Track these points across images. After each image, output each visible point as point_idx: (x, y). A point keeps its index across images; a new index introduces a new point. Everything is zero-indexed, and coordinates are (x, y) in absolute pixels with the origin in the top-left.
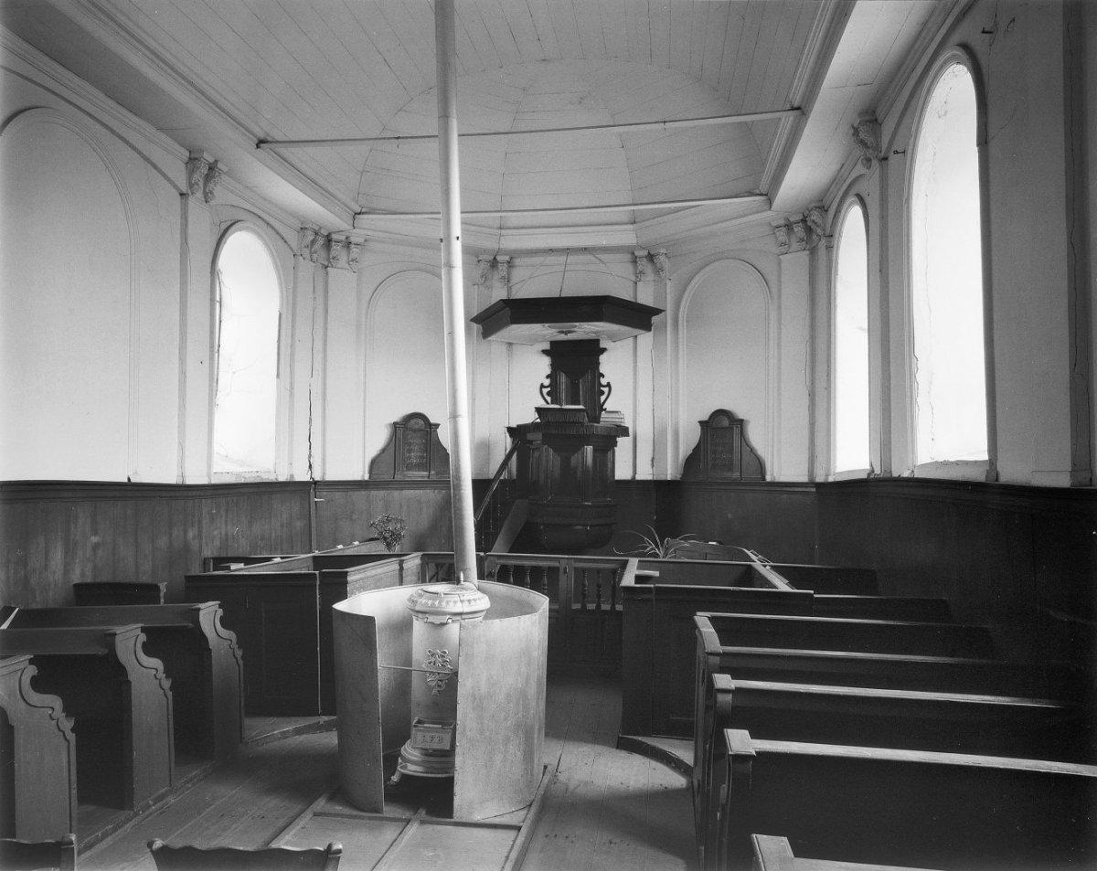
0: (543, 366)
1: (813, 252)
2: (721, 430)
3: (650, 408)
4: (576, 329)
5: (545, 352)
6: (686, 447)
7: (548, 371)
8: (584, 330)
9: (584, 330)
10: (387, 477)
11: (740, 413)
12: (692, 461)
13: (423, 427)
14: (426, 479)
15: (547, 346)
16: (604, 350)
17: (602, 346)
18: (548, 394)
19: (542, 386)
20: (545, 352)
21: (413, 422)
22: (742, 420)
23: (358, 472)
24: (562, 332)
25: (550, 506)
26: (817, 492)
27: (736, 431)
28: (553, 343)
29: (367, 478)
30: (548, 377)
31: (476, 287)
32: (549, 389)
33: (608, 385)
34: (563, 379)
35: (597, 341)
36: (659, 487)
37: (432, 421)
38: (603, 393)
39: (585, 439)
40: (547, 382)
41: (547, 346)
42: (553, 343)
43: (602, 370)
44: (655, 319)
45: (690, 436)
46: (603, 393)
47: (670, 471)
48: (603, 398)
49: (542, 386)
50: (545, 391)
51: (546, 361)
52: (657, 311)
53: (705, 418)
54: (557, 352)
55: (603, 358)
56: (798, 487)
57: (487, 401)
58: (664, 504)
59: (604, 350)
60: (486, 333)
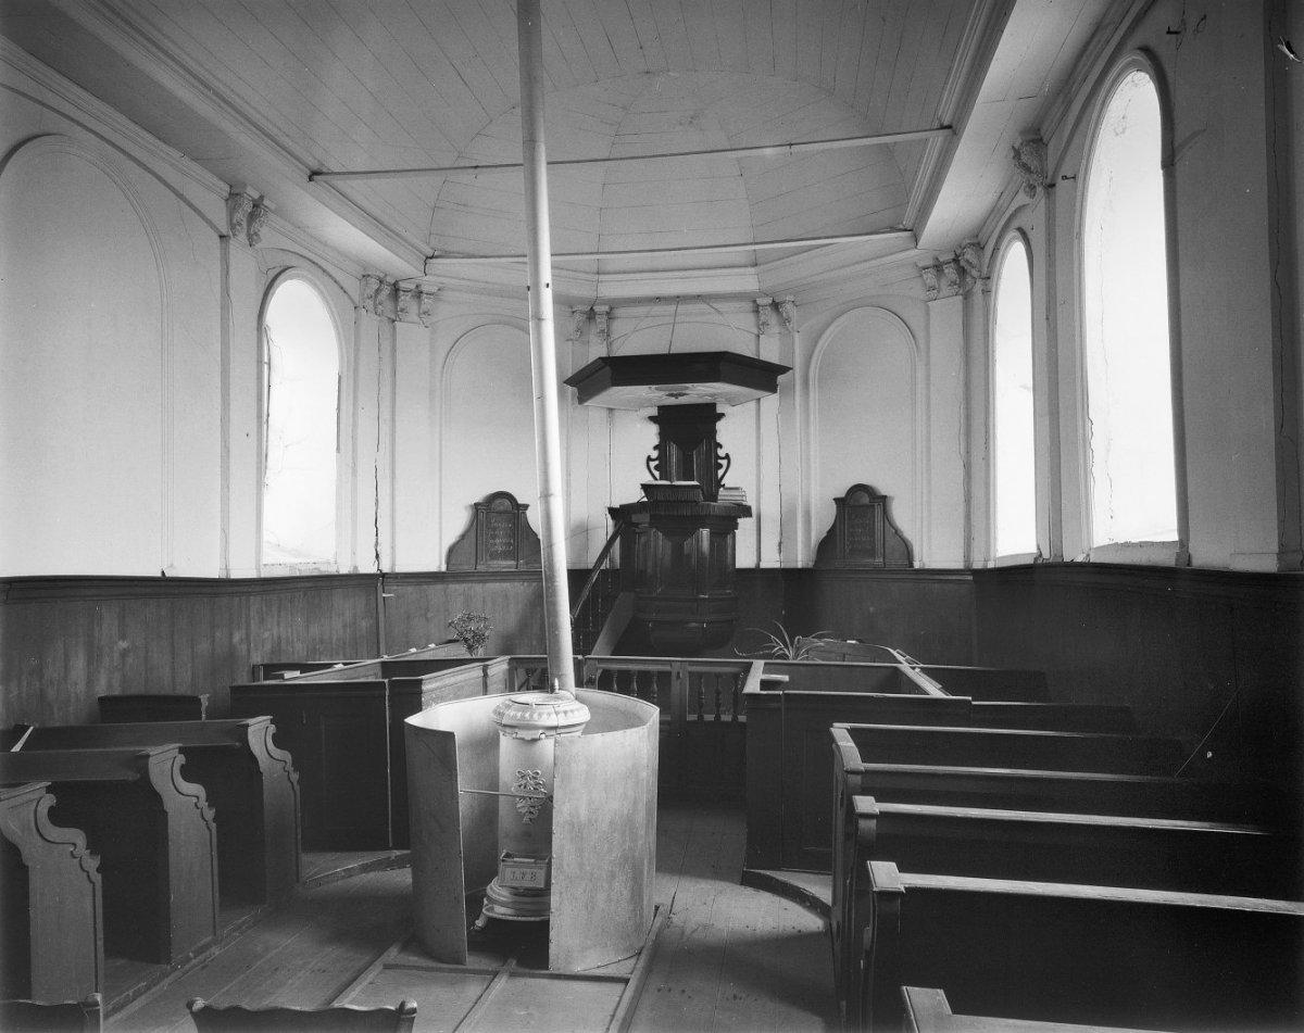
0: (650, 435)
1: (967, 296)
2: (861, 508)
5: (652, 419)
7: (656, 441)
8: (698, 392)
11: (883, 490)
12: (826, 546)
15: (654, 412)
16: (722, 415)
18: (656, 468)
19: (649, 459)
21: (498, 501)
23: (434, 562)
24: (672, 395)
27: (878, 511)
29: (444, 569)
30: (655, 448)
31: (570, 343)
32: (657, 462)
33: (727, 457)
34: (673, 450)
35: (713, 406)
36: (788, 575)
38: (721, 466)
39: (701, 521)
40: (655, 454)
41: (654, 412)
44: (781, 379)
45: (823, 518)
46: (721, 466)
47: (801, 558)
48: (720, 472)
49: (649, 459)
50: (653, 464)
51: (654, 429)
52: (784, 370)
53: (842, 494)
54: (667, 419)
55: (720, 425)
57: (586, 477)
60: (583, 397)
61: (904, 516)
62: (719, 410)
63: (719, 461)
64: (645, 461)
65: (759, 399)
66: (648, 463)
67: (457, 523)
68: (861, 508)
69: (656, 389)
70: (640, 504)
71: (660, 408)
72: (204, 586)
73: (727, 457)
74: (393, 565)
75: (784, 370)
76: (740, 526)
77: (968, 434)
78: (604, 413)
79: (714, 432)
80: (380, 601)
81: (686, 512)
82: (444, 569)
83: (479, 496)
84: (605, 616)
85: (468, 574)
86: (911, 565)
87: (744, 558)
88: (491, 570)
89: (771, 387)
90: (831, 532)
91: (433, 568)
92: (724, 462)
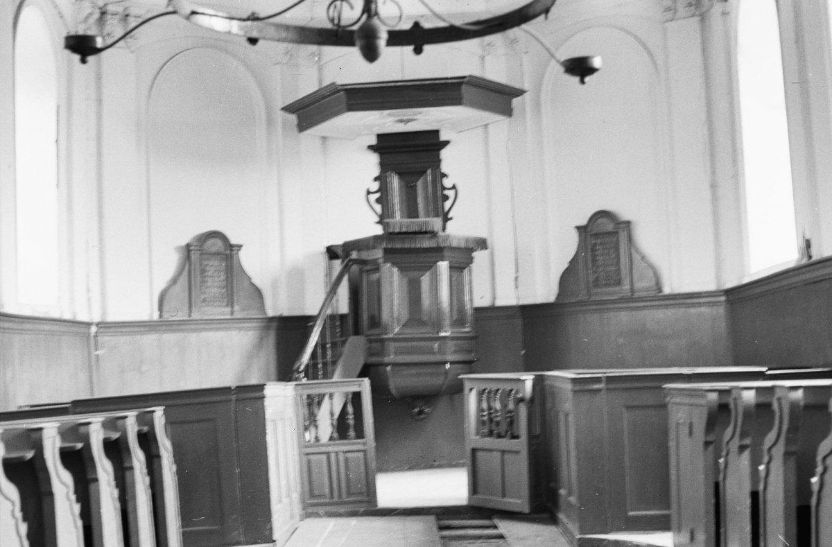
0: (372, 163)
1: (703, 18)
2: (603, 236)
3: (512, 220)
4: (418, 117)
5: (371, 147)
6: (560, 263)
7: (376, 172)
8: (423, 119)
9: (423, 119)
10: (182, 316)
11: (625, 215)
12: (566, 278)
13: (222, 249)
14: (228, 317)
15: (374, 141)
16: (446, 143)
17: (443, 137)
18: (378, 201)
19: (369, 193)
20: (371, 147)
21: (210, 242)
22: (628, 223)
23: (146, 310)
24: (401, 121)
25: (383, 346)
26: (728, 301)
27: (623, 236)
28: (380, 137)
29: (156, 317)
30: (376, 179)
31: (278, 67)
32: (378, 195)
33: (454, 187)
34: (395, 181)
35: (436, 132)
36: (530, 314)
37: (233, 241)
38: (446, 198)
39: (438, 252)
40: (375, 186)
41: (374, 141)
42: (380, 137)
43: (444, 168)
44: (516, 102)
45: (564, 248)
46: (446, 198)
47: (543, 290)
48: (447, 204)
49: (369, 193)
50: (374, 197)
51: (374, 159)
52: (519, 93)
53: (583, 222)
54: (387, 146)
55: (444, 153)
56: (692, 298)
57: (309, 209)
58: (534, 332)
59: (446, 143)
60: (303, 126)
61: (651, 241)
62: (443, 137)
63: (446, 192)
64: (364, 193)
65: (486, 126)
66: (368, 200)
67: (168, 264)
68: (603, 236)
69: (389, 114)
70: (376, 238)
71: (380, 136)
72: (781, 280)
73: (454, 187)
74: (104, 313)
75: (519, 93)
76: (475, 260)
77: (712, 156)
78: (318, 142)
79: (439, 161)
80: (93, 357)
81: (426, 243)
82: (156, 317)
83: (187, 236)
84: (334, 363)
85: (182, 323)
86: (660, 290)
87: (480, 297)
88: (206, 317)
89: (507, 111)
90: (573, 262)
91: (792, 265)
92: (451, 193)
